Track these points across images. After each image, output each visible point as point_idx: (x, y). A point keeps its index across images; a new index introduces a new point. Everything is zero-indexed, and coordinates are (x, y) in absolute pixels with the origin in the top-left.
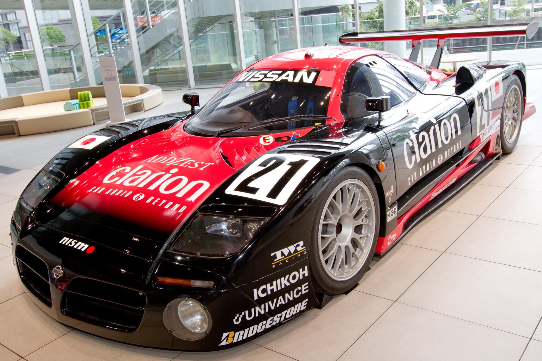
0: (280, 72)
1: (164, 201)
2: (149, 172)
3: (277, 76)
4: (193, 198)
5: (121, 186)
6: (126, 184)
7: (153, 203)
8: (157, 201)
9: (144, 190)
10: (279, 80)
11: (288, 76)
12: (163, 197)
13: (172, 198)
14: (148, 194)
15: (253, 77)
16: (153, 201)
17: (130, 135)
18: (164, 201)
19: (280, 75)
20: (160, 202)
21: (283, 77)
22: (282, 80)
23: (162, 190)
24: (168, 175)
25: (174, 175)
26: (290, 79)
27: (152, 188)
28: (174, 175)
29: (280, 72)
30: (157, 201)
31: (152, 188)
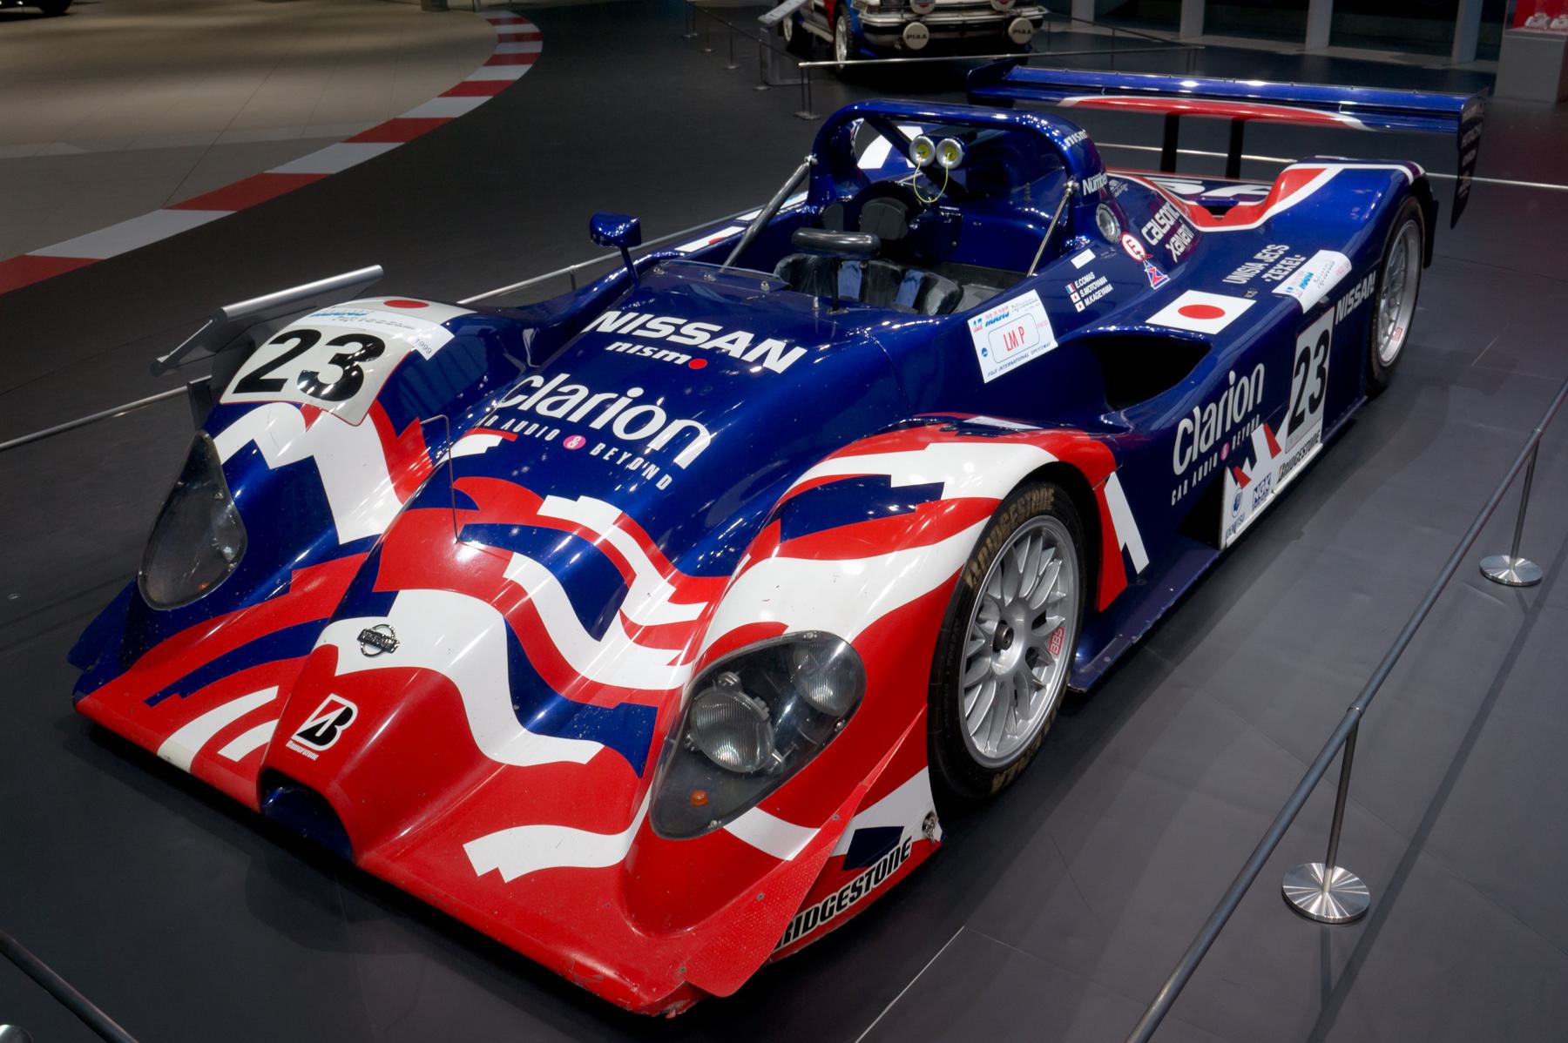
0: (716, 328)
1: (626, 455)
2: (1212, 406)
3: (708, 336)
4: (684, 459)
5: (1203, 457)
6: (1204, 449)
7: (606, 457)
8: (611, 453)
9: (583, 427)
10: (708, 346)
11: (733, 342)
12: (624, 445)
13: (636, 448)
14: (593, 437)
15: (643, 327)
16: (603, 452)
17: (705, 1008)
18: (626, 455)
19: (714, 335)
20: (618, 455)
21: (721, 343)
22: (715, 349)
23: (619, 430)
24: (624, 401)
25: (636, 402)
26: (736, 351)
27: (598, 424)
28: (636, 402)
29: (716, 328)
30: (611, 453)
31: (598, 424)
